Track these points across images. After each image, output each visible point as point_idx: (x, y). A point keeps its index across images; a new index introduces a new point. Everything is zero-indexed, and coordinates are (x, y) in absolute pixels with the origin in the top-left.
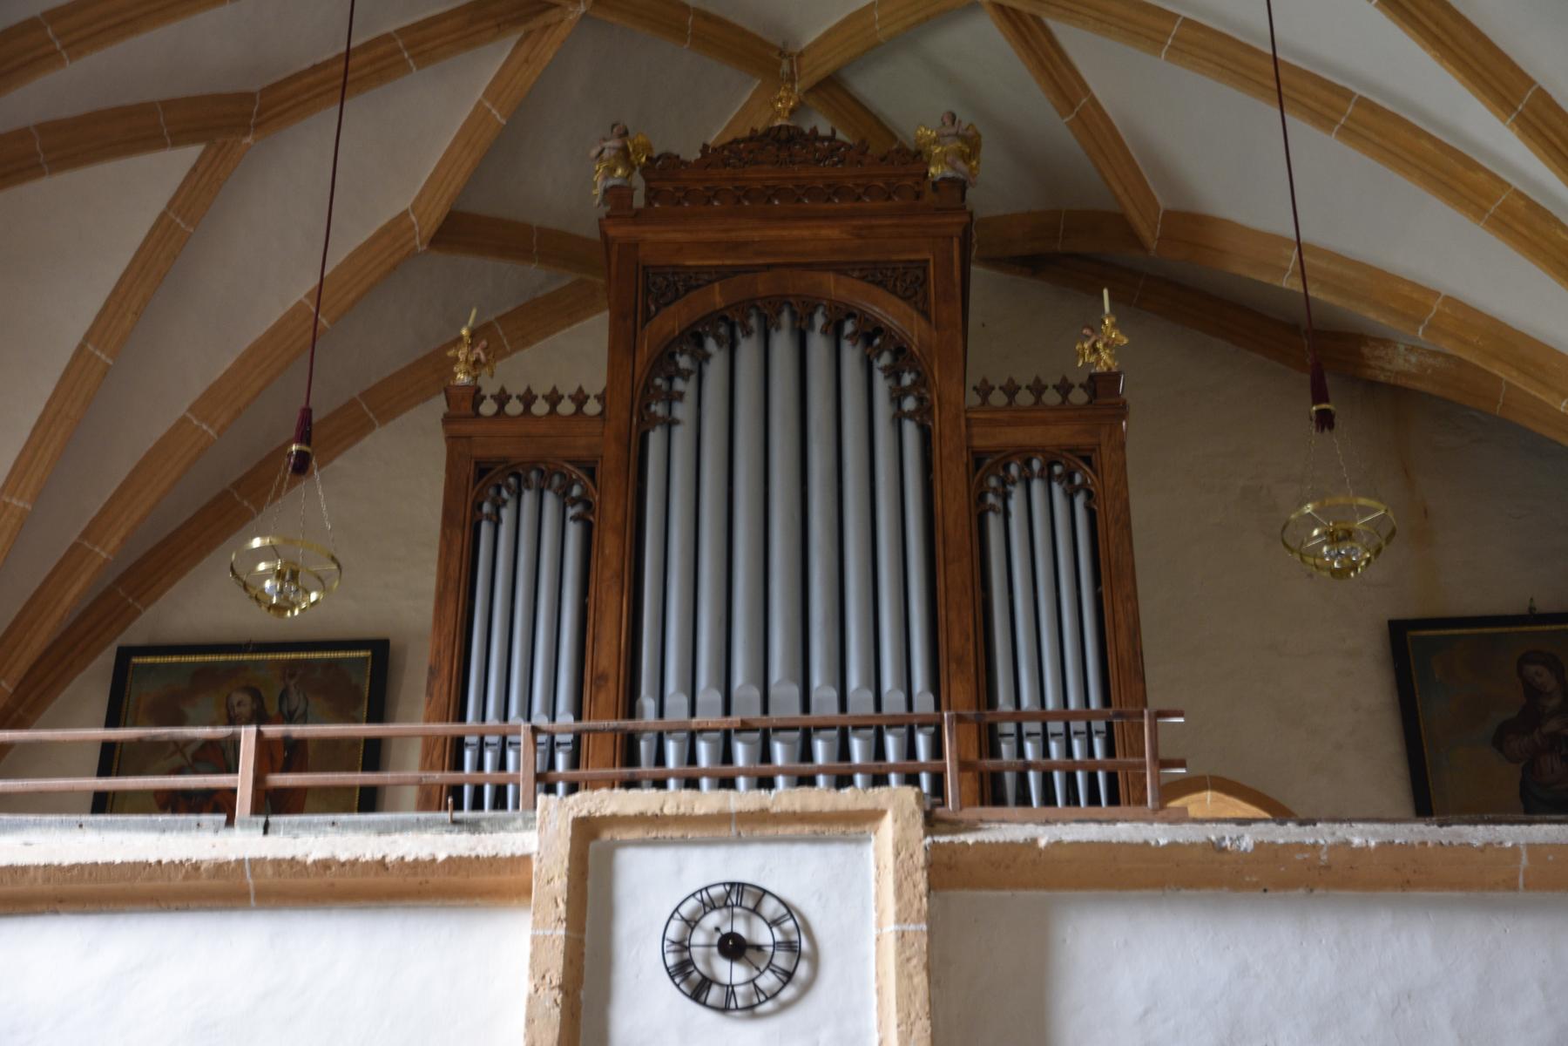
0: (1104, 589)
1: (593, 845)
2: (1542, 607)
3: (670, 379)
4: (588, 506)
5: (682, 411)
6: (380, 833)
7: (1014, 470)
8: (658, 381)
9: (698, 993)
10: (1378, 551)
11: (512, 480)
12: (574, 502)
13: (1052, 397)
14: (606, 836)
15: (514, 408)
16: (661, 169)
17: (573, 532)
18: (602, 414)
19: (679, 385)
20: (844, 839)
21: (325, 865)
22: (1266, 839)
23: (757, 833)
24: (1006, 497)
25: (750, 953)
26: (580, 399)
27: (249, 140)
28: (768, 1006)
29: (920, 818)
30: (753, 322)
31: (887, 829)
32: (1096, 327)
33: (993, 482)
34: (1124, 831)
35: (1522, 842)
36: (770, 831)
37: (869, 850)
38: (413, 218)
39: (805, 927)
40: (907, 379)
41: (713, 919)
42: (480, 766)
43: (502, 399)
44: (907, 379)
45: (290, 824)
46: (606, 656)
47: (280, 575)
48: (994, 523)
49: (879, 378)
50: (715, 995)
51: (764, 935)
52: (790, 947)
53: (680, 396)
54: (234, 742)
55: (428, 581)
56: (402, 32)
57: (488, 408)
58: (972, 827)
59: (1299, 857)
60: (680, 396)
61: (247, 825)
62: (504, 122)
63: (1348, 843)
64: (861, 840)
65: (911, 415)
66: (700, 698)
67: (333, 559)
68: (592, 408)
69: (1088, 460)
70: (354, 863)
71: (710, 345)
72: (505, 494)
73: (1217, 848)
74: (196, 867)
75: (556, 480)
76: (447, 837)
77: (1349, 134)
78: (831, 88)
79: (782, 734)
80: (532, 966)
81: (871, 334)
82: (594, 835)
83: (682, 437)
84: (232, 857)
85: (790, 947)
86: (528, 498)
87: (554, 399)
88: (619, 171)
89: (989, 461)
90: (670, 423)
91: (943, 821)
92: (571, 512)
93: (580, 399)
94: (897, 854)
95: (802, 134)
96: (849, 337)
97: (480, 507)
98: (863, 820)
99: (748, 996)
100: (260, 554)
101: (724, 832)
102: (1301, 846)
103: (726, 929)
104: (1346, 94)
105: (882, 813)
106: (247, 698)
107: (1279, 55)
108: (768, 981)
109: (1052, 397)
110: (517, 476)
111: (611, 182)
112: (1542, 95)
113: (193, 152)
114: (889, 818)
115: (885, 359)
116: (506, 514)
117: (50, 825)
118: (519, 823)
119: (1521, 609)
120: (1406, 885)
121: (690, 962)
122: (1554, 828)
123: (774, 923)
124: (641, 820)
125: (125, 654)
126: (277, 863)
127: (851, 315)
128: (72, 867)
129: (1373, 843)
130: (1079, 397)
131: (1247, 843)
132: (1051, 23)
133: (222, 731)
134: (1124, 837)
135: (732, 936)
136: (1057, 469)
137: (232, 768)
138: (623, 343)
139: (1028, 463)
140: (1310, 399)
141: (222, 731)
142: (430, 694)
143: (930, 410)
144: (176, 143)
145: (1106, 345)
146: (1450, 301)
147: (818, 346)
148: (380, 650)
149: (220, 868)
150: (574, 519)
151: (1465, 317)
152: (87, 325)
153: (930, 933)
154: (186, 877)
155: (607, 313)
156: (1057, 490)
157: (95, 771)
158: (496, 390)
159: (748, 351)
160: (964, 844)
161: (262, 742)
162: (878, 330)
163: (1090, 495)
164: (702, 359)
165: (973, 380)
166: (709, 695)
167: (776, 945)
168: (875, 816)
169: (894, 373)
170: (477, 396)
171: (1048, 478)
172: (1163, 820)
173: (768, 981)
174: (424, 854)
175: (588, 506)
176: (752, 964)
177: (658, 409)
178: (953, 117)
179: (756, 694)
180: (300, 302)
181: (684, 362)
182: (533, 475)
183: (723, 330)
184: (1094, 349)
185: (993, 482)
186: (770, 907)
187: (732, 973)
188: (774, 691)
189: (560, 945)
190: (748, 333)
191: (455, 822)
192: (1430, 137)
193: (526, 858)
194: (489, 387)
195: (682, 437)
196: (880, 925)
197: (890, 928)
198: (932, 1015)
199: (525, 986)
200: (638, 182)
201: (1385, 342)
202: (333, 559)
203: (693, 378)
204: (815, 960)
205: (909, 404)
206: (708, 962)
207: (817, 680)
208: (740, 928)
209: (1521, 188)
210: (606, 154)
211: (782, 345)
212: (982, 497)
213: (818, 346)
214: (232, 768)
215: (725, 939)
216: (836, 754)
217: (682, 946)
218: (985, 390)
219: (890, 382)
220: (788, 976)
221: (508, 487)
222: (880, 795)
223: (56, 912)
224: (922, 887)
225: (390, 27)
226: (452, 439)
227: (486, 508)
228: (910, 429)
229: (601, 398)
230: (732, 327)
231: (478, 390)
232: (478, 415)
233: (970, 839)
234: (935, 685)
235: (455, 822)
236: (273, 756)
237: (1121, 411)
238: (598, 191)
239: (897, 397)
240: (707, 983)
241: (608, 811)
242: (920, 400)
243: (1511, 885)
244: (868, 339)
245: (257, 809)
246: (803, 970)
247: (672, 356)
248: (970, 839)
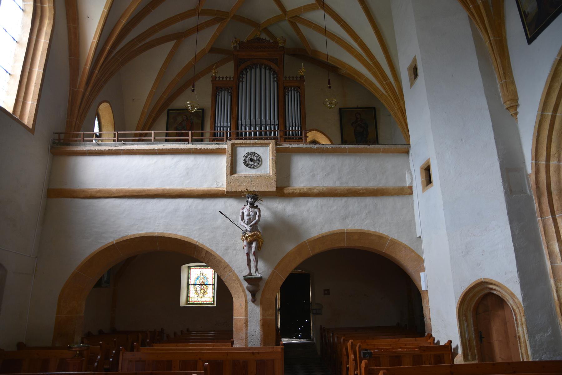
0: (301, 106)
1: (234, 147)
2: (359, 106)
3: (242, 75)
4: (231, 93)
5: (244, 80)
6: (207, 145)
7: (289, 89)
8: (241, 75)
9: (247, 166)
10: (335, 105)
11: (221, 89)
12: (230, 93)
13: (295, 79)
14: (235, 146)
15: (221, 79)
16: (241, 44)
17: (229, 97)
18: (233, 80)
19: (244, 76)
20: (266, 146)
21: (200, 149)
22: (318, 147)
23: (254, 146)
24: (288, 93)
25: (254, 161)
26: (230, 78)
27: (183, 39)
28: (256, 167)
29: (275, 144)
30: (254, 67)
31: (271, 145)
32: (301, 68)
33: (287, 91)
34: (300, 146)
35: (348, 147)
36: (256, 145)
37: (269, 148)
38: (206, 49)
39: (260, 157)
40: (275, 76)
41: (249, 156)
42: (218, 130)
43: (219, 78)
44: (275, 76)
45: (196, 144)
46: (234, 115)
47: (191, 106)
48: (287, 96)
49: (271, 75)
50: (249, 166)
51: (255, 159)
52: (259, 160)
53: (244, 78)
54: (188, 133)
55: (210, 100)
56: (204, 22)
57: (217, 79)
58: (282, 145)
59: (322, 149)
60: (244, 78)
61: (190, 144)
62: (218, 35)
63: (327, 147)
64: (268, 147)
65: (276, 81)
66: (247, 121)
67: (198, 104)
68: (232, 79)
69: (299, 88)
70: (204, 149)
71: (248, 70)
72: (220, 91)
73: (311, 148)
74: (185, 149)
75: (227, 89)
76: (216, 145)
77: (337, 42)
78: (266, 30)
79: (258, 126)
80: (227, 162)
81: (270, 69)
82: (234, 146)
83: (244, 83)
84: (189, 148)
85: (259, 160)
86: (223, 92)
87: (226, 78)
88: (235, 44)
89: (286, 88)
90: (242, 81)
91: (278, 144)
92: (229, 94)
93: (230, 78)
94: (272, 149)
95: (261, 38)
96: (267, 69)
97: (217, 93)
98: (267, 145)
99: (253, 166)
100: (189, 104)
101: (250, 145)
102: (322, 148)
103: (251, 158)
104: (336, 36)
105: (270, 143)
106: (185, 117)
107: (326, 29)
108: (256, 164)
109: (295, 79)
110: (221, 89)
111: (234, 46)
112: (361, 40)
113: (175, 41)
114: (271, 144)
115: (272, 73)
116: (220, 94)
117: (166, 143)
118: (224, 144)
119: (356, 107)
120: (334, 152)
121: (246, 162)
122: (352, 145)
123: (256, 157)
124: (240, 144)
125: (169, 110)
126: (195, 149)
127: (267, 66)
128: (170, 149)
129: (330, 147)
130: (299, 79)
131: (315, 147)
132: (296, 23)
133: (187, 131)
134: (300, 147)
135: (251, 158)
136: (295, 89)
137: (188, 136)
138: (237, 67)
139: (291, 88)
140: (328, 84)
141: (187, 131)
142: (211, 120)
143: (278, 81)
144: (173, 40)
145: (302, 72)
146: (349, 65)
147: (263, 70)
148: (203, 110)
149: (188, 149)
150: (230, 95)
151: (351, 68)
152: (162, 65)
153: (276, 158)
154: (184, 150)
155: (233, 61)
156: (295, 92)
157: (166, 130)
158: (218, 77)
159: (253, 71)
160: (280, 147)
161: (192, 133)
162: (271, 68)
163: (300, 93)
164: (247, 72)
165: (284, 76)
166: (248, 121)
167: (257, 160)
168: (269, 144)
169: (273, 75)
170: (216, 77)
171: (294, 90)
172: (305, 144)
173: (256, 164)
174: (213, 148)
175: (231, 93)
176: (254, 162)
177: (241, 79)
178: (282, 37)
179: (254, 120)
180: (190, 61)
181: (244, 72)
182: (224, 89)
183: (250, 68)
184: (301, 72)
185: (287, 91)
186: (256, 155)
187: (252, 163)
188: (257, 120)
189: (230, 160)
190: (253, 69)
191: (216, 144)
192: (347, 43)
193: (226, 149)
194: (217, 76)
195: (244, 83)
196: (270, 157)
197: (271, 158)
198: (276, 169)
199: (226, 165)
200: (238, 46)
201: (341, 69)
202: (198, 104)
203: (246, 75)
204: (262, 162)
205: (275, 79)
206: (248, 162)
207: (262, 118)
208: (252, 158)
209: (359, 52)
210: (233, 41)
211: (258, 70)
212: (285, 93)
213: (263, 70)
214: (188, 136)
215: (251, 159)
216: (265, 129)
217: (245, 160)
218: (286, 78)
219: (273, 76)
220: (258, 164)
221: (221, 91)
222: (270, 141)
223: (168, 154)
224: (275, 153)
225: (203, 22)
226: (213, 84)
227: (218, 94)
228: (275, 83)
229: (233, 78)
230: (251, 67)
231: (216, 76)
232: (216, 80)
233: (281, 147)
234: (278, 119)
235: (216, 144)
236: (192, 134)
237: (304, 81)
238: (232, 47)
239: (274, 78)
240: (248, 164)
241: (236, 143)
242: (277, 79)
243: (346, 152)
244: (270, 70)
245: (192, 141)
246: (260, 163)
247: (243, 71)
248: (281, 147)
